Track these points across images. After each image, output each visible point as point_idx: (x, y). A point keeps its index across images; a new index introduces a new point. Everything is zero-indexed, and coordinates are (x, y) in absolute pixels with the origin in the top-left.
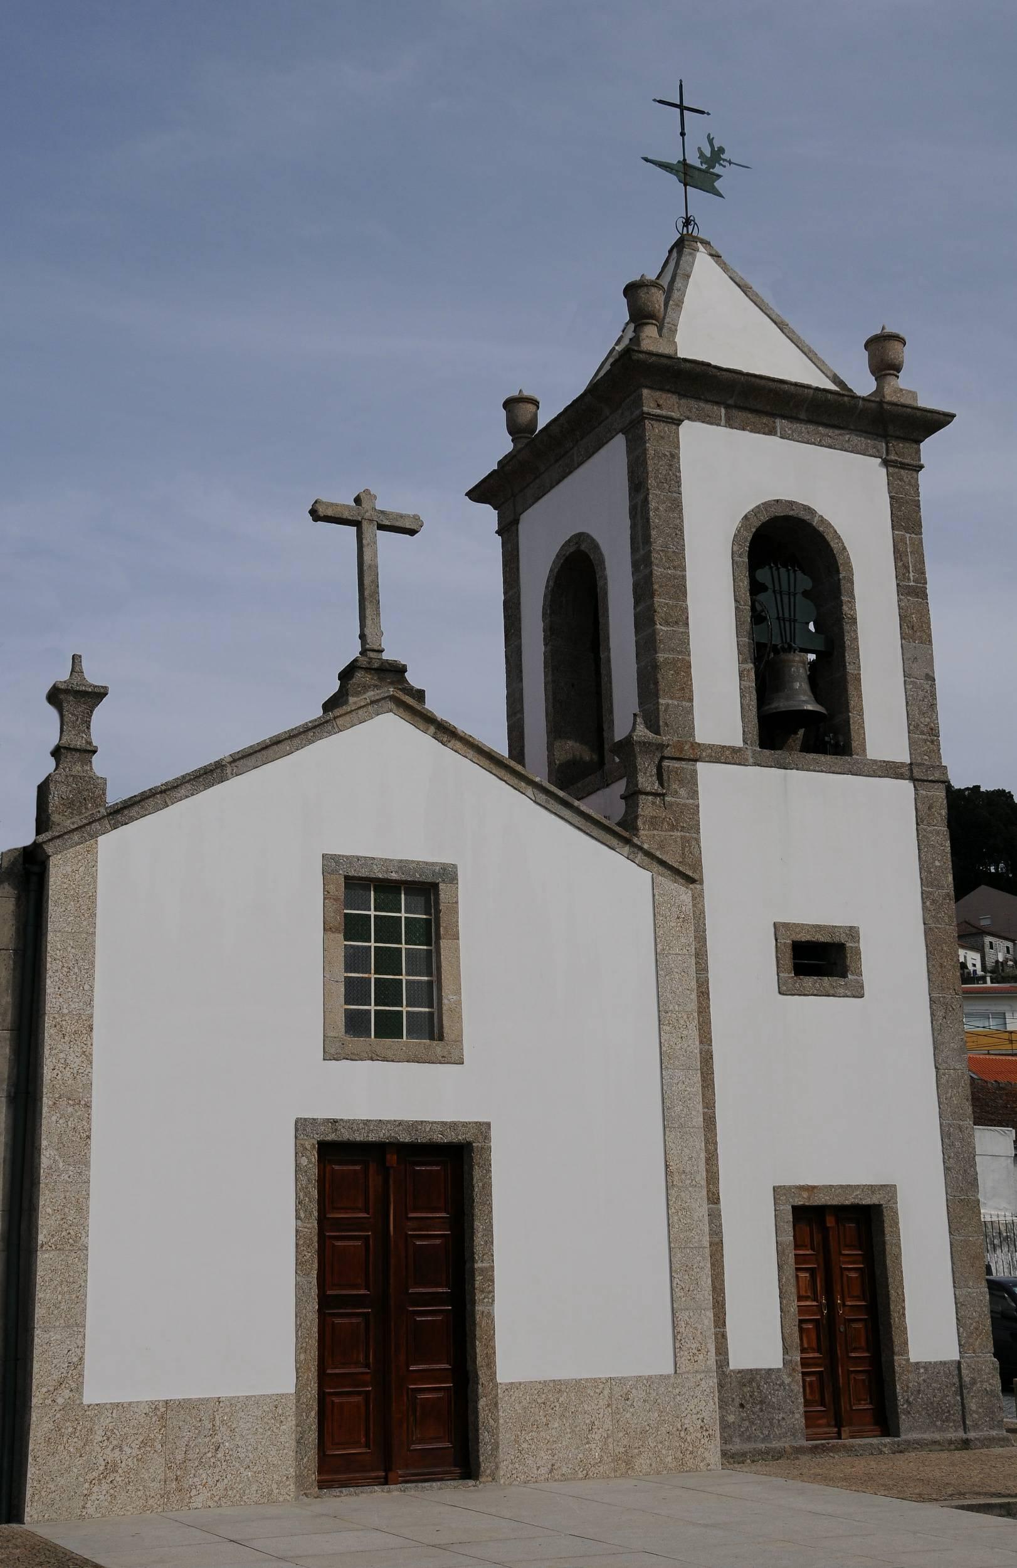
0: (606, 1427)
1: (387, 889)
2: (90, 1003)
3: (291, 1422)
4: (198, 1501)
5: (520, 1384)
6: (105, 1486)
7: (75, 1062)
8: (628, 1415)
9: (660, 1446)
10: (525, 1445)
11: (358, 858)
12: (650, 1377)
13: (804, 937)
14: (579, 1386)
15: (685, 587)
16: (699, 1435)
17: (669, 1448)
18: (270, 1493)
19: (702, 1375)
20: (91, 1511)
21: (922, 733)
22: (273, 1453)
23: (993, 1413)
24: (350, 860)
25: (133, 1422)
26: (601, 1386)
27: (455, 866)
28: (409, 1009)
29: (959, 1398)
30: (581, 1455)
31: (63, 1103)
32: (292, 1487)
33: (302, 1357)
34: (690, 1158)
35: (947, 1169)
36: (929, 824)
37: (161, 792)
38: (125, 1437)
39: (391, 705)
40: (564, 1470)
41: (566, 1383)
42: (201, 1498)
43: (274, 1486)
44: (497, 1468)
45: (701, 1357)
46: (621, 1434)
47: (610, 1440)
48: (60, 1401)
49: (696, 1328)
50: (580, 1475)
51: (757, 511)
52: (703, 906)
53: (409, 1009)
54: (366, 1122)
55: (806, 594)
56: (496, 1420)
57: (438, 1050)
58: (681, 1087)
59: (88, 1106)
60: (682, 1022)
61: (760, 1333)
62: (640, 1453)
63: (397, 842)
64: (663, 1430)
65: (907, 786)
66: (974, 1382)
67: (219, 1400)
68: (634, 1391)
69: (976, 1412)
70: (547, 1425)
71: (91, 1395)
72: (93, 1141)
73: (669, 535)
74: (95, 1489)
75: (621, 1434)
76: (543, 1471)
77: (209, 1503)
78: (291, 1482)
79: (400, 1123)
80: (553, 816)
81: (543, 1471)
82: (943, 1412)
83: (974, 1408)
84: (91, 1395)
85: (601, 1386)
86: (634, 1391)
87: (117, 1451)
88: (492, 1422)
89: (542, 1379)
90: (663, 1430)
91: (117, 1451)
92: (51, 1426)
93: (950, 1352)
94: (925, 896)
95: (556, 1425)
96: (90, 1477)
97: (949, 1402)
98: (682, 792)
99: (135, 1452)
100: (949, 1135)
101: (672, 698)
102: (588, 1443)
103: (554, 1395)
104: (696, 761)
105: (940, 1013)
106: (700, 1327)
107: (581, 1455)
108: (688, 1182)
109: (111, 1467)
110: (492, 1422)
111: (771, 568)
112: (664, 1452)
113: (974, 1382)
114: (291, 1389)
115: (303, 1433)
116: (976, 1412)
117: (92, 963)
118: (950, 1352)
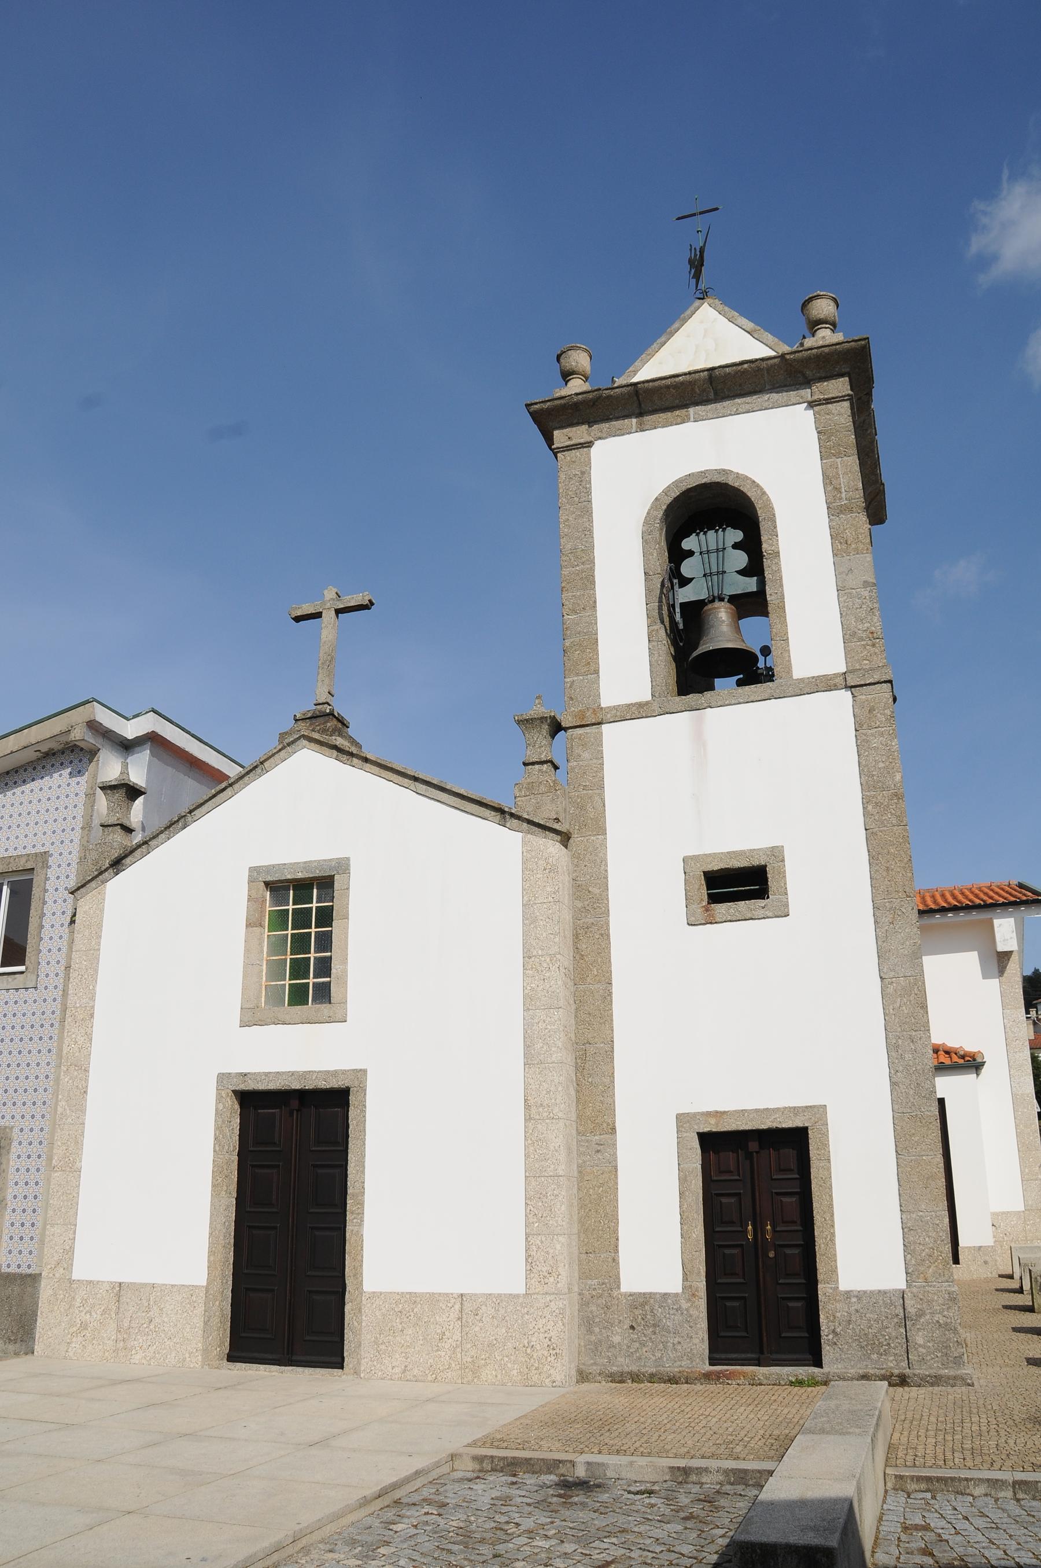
0: (455, 1337)
1: (302, 887)
2: (93, 999)
3: (200, 1310)
4: (137, 1358)
5: (381, 1293)
6: (80, 1339)
7: (81, 1040)
8: (477, 1329)
9: (506, 1359)
10: (383, 1347)
11: (274, 866)
12: (500, 1295)
13: (715, 866)
14: (433, 1299)
15: (593, 576)
16: (546, 1353)
17: (514, 1363)
18: (184, 1360)
19: (552, 1297)
20: (71, 1354)
21: (861, 639)
22: (188, 1330)
23: (947, 1347)
24: (269, 869)
25: (99, 1296)
26: (453, 1301)
27: (252, 869)
28: (316, 980)
29: (903, 1330)
30: (431, 1361)
31: (72, 1068)
32: (200, 1357)
33: (212, 1258)
34: (548, 1092)
35: (893, 1084)
36: (870, 728)
37: (519, 818)
38: (93, 1306)
39: (305, 742)
40: (416, 1372)
41: (421, 1295)
42: (138, 1357)
43: (187, 1355)
44: (359, 1363)
45: (551, 1279)
46: (469, 1346)
47: (459, 1350)
48: (57, 1275)
49: (548, 1253)
50: (430, 1378)
51: (769, 506)
52: (605, 854)
53: (316, 980)
54: (267, 1074)
55: (736, 546)
56: (360, 1323)
57: (326, 1011)
58: (542, 1025)
59: (87, 1071)
60: (545, 965)
61: (659, 1248)
62: (486, 1365)
63: (297, 852)
64: (509, 1345)
65: (845, 697)
66: (921, 1314)
67: (153, 1286)
68: (483, 1307)
69: (923, 1346)
70: (402, 1331)
71: (79, 1273)
72: (89, 1097)
73: (577, 538)
74: (74, 1339)
75: (469, 1346)
76: (397, 1370)
77: (144, 1361)
78: (199, 1353)
79: (293, 1073)
80: (433, 801)
81: (397, 1370)
82: (881, 1345)
83: (920, 1340)
84: (79, 1273)
85: (453, 1301)
86: (483, 1307)
87: (88, 1315)
88: (356, 1324)
89: (400, 1291)
90: (509, 1345)
91: (88, 1315)
92: (51, 1292)
93: (894, 1279)
94: (866, 802)
95: (410, 1332)
96: (71, 1331)
97: (889, 1334)
98: (586, 755)
99: (99, 1317)
100: (897, 1047)
101: (577, 675)
102: (438, 1350)
103: (412, 1306)
104: (600, 723)
105: (885, 920)
106: (551, 1251)
107: (431, 1361)
108: (545, 1114)
109: (84, 1326)
110: (356, 1324)
111: (698, 535)
112: (509, 1365)
113: (921, 1314)
114: (204, 1282)
115: (209, 1317)
116: (923, 1346)
117: (96, 971)
118: (894, 1279)
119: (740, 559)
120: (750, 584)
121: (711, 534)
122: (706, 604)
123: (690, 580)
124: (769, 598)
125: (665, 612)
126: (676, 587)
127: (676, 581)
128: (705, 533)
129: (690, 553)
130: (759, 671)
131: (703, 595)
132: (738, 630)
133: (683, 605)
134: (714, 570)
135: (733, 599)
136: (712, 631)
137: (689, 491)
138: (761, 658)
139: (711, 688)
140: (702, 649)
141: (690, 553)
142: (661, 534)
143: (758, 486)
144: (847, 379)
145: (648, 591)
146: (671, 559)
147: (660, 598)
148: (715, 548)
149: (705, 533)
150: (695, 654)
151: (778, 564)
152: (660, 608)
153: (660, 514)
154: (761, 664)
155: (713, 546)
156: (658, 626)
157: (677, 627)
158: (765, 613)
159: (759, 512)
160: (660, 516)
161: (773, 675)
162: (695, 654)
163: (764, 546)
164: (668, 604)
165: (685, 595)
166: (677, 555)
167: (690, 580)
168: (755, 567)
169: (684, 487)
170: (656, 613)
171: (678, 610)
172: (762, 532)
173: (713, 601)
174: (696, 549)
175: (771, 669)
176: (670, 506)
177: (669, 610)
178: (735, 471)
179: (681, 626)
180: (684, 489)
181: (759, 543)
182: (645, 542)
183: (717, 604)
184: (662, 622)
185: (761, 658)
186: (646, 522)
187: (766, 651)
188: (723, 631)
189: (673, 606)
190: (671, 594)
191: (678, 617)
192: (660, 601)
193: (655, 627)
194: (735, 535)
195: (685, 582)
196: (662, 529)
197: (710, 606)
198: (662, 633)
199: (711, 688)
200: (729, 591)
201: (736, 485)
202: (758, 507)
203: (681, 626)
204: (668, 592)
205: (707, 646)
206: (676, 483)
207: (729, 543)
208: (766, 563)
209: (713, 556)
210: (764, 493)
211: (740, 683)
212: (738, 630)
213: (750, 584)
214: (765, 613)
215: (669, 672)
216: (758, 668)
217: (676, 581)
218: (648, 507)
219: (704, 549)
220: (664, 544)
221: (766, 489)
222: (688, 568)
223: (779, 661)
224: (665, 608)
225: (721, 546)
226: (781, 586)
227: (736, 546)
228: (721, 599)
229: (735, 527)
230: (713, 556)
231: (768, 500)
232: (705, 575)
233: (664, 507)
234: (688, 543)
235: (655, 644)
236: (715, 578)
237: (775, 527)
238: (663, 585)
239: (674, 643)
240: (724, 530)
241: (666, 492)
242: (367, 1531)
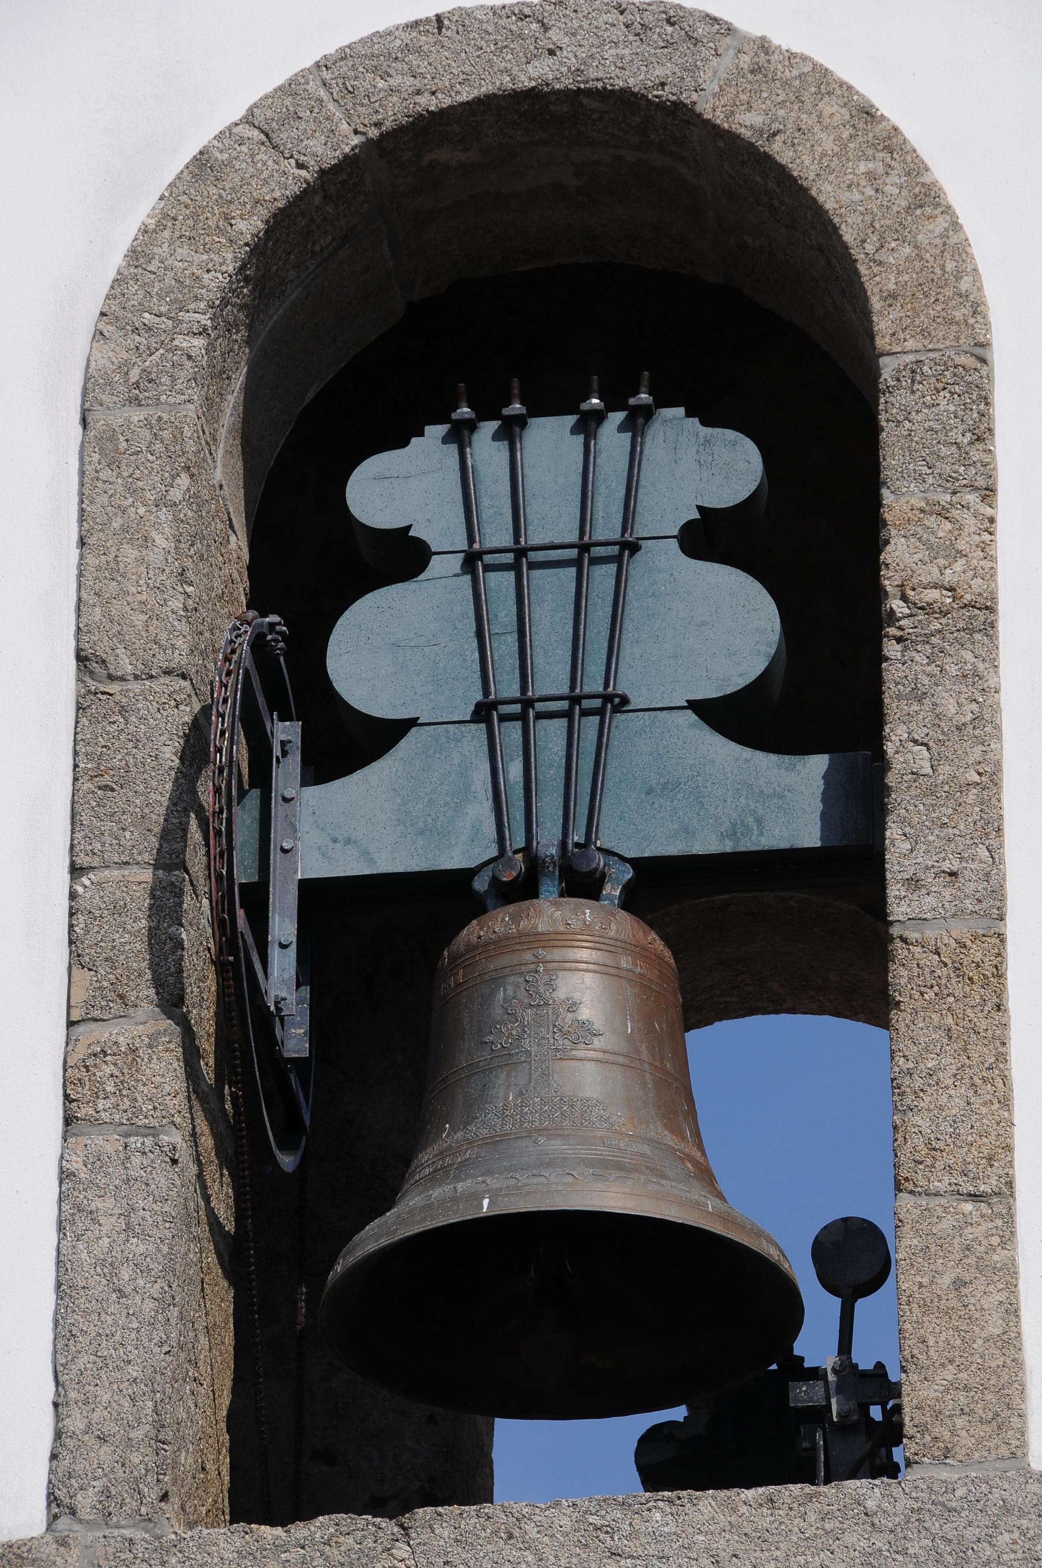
55: (708, 536)
111: (460, 435)
119: (726, 626)
120: (784, 801)
121: (550, 438)
122: (477, 908)
123: (377, 737)
124: (900, 905)
125: (197, 933)
126: (286, 774)
127: (285, 732)
128: (511, 432)
129: (400, 556)
130: (803, 1394)
131: (463, 842)
132: (674, 1096)
133: (315, 895)
134: (551, 677)
135: (662, 889)
136: (504, 1091)
137: (426, 130)
138: (820, 1307)
139: (465, 1480)
140: (423, 1207)
141: (400, 556)
142: (210, 406)
143: (892, 143)
144: (520, 722)
145: (94, 778)
146: (266, 585)
147: (172, 835)
148: (578, 533)
149: (511, 432)
150: (375, 1236)
151: (979, 682)
152: (165, 906)
153: (216, 267)
154: (815, 1344)
155: (552, 522)
156: (143, 1024)
157: (269, 1042)
158: (868, 999)
159: (885, 324)
160: (214, 283)
161: (893, 1431)
162: (375, 1236)
163: (900, 556)
164: (223, 883)
165: (344, 830)
166: (308, 558)
167: (377, 737)
168: (828, 687)
169: (397, 98)
170: (130, 938)
171: (283, 925)
172: (894, 458)
173: (523, 889)
174: (439, 527)
175: (879, 1384)
176: (289, 225)
177: (224, 926)
178: (750, 22)
179: (295, 1040)
180: (394, 112)
181: (866, 531)
182: (101, 447)
183: (551, 912)
184: (172, 1000)
185: (820, 1307)
186: (115, 317)
187: (856, 1258)
188: (578, 1091)
189: (257, 899)
190: (245, 819)
191: (281, 977)
192: (170, 859)
193: (120, 1033)
194: (708, 464)
195: (343, 742)
196: (221, 375)
197: (500, 922)
198: (164, 1075)
199: (465, 1480)
200: (640, 828)
201: (747, 122)
202: (877, 284)
203: (295, 1040)
204: (228, 801)
205: (454, 1189)
206: (343, 71)
207: (667, 509)
208: (900, 666)
209: (552, 589)
210: (928, 198)
211: (667, 1466)
212: (674, 1096)
213: (784, 801)
214: (868, 999)
215: (181, 1339)
216: (798, 1370)
217: (285, 732)
218: (142, 209)
219: (497, 534)
220: (225, 472)
221: (946, 172)
222: (383, 651)
223: (936, 1335)
224: (198, 911)
225: (607, 527)
226: (991, 829)
227: (708, 536)
228: (582, 884)
229: (710, 412)
230: (552, 589)
231: (954, 247)
232: (483, 713)
233: (250, 226)
234: (395, 487)
235: (108, 1144)
236: (551, 735)
237: (982, 435)
238: (195, 749)
239: (240, 1147)
240: (637, 422)
241: (266, 125)
242: (211, 1331)
